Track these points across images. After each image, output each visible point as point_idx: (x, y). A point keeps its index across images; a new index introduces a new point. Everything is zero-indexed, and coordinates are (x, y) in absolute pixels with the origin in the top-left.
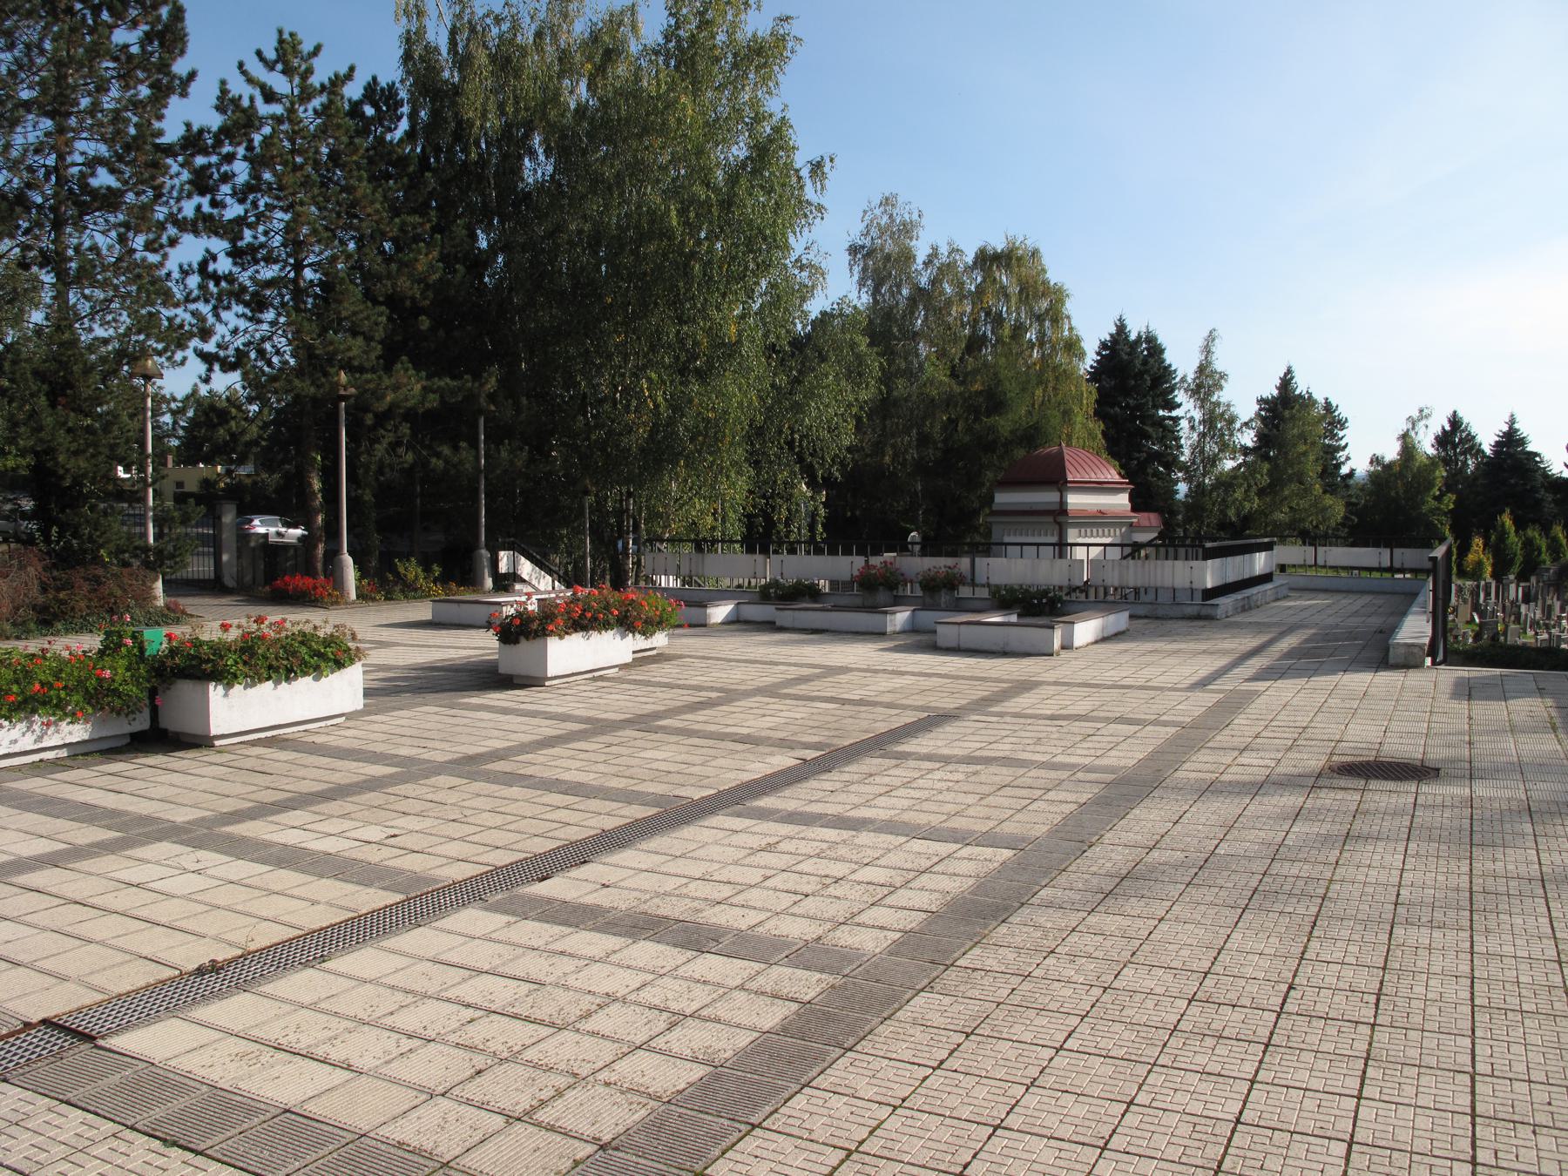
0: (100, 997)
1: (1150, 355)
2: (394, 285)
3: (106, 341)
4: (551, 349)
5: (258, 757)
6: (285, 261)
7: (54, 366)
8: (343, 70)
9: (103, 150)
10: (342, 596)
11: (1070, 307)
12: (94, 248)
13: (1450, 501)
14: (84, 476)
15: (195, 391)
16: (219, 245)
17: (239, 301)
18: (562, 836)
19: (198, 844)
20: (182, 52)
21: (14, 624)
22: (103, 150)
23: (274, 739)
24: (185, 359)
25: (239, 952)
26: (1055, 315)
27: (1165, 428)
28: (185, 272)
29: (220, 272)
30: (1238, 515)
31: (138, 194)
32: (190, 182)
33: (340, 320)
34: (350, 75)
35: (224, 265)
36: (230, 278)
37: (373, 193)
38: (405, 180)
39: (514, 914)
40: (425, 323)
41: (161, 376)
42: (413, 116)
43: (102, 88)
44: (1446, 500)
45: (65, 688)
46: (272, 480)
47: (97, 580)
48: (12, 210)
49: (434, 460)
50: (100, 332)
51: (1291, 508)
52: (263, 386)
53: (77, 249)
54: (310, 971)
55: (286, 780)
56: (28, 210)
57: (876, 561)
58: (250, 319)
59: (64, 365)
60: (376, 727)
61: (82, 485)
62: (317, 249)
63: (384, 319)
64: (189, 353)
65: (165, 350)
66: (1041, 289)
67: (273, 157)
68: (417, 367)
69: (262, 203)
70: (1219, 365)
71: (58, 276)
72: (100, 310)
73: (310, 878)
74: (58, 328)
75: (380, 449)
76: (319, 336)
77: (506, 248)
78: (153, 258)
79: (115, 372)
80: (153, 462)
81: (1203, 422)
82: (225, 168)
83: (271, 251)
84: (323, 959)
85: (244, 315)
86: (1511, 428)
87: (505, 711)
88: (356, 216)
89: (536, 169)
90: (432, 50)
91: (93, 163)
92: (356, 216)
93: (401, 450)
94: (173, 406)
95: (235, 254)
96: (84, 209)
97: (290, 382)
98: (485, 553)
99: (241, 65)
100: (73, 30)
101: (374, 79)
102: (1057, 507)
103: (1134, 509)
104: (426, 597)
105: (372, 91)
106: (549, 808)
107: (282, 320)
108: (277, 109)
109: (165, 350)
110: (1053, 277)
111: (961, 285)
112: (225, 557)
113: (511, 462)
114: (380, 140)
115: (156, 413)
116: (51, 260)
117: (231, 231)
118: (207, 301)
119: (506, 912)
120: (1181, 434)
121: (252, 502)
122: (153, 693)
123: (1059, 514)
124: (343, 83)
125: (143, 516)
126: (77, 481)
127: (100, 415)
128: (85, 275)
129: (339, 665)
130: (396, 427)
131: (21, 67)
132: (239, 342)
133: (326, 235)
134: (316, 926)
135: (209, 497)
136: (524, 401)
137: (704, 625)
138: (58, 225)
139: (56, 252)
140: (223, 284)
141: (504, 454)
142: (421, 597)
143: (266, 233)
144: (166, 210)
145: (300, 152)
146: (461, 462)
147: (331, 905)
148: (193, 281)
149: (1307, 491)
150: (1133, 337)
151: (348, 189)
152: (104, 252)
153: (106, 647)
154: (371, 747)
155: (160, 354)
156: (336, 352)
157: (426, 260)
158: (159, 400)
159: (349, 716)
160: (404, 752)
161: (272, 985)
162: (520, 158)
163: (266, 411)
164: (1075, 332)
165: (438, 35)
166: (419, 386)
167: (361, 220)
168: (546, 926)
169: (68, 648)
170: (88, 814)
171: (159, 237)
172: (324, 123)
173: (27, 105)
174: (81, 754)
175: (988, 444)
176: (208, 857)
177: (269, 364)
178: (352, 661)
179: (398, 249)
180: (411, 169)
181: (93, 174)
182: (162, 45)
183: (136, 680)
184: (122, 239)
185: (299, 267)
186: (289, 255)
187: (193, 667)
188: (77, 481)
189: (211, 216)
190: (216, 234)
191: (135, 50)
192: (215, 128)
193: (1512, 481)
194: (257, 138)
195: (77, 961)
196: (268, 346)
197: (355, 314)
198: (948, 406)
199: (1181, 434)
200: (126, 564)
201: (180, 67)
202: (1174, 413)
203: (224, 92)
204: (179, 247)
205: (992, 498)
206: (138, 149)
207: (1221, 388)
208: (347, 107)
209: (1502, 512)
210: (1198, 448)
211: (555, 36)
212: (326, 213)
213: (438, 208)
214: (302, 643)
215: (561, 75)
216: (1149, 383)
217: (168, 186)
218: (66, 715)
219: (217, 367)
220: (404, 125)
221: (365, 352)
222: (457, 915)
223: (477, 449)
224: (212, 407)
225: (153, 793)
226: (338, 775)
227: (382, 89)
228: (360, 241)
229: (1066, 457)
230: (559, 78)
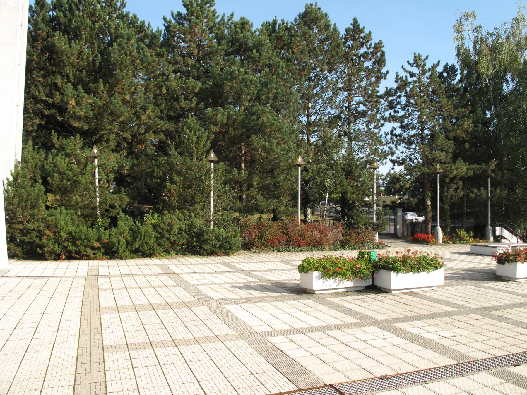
0: (348, 380)
2: (456, 133)
3: (362, 158)
4: (516, 152)
5: (406, 299)
6: (418, 128)
7: (347, 166)
8: (436, 63)
9: (361, 99)
12: (359, 129)
14: (355, 200)
15: (389, 173)
16: (397, 125)
17: (403, 142)
18: (525, 347)
19: (384, 328)
20: (384, 65)
21: (334, 246)
22: (361, 99)
23: (411, 292)
24: (386, 162)
25: (395, 373)
28: (386, 135)
29: (397, 134)
31: (372, 111)
32: (387, 106)
33: (437, 146)
34: (438, 64)
35: (398, 131)
36: (400, 135)
37: (448, 102)
38: (459, 96)
39: (503, 379)
40: (467, 146)
41: (379, 168)
42: (462, 73)
43: (361, 81)
45: (346, 269)
46: (414, 201)
47: (358, 233)
48: (336, 120)
49: (471, 194)
50: (361, 155)
52: (411, 170)
53: (354, 130)
54: (420, 386)
55: (415, 308)
56: (341, 120)
58: (407, 148)
59: (350, 166)
60: (448, 292)
61: (355, 203)
62: (429, 123)
63: (452, 145)
64: (388, 160)
65: (380, 160)
67: (413, 94)
68: (465, 161)
69: (410, 110)
71: (349, 139)
72: (361, 148)
73: (422, 348)
74: (349, 155)
75: (451, 190)
76: (430, 152)
77: (497, 116)
78: (376, 131)
79: (365, 167)
82: (398, 100)
83: (413, 125)
84: (425, 382)
85: (405, 147)
87: (499, 290)
88: (442, 111)
89: (508, 87)
90: (468, 50)
91: (359, 103)
92: (442, 111)
93: (459, 191)
94: (382, 177)
95: (402, 127)
96: (356, 118)
97: (420, 168)
98: (490, 228)
99: (402, 67)
100: (353, 65)
101: (447, 64)
104: (468, 243)
105: (446, 68)
106: (518, 334)
107: (417, 148)
108: (415, 79)
109: (380, 160)
112: (398, 227)
113: (501, 194)
114: (450, 84)
115: (377, 179)
116: (347, 134)
117: (400, 120)
118: (393, 143)
119: (500, 377)
121: (407, 208)
122: (373, 273)
124: (436, 67)
125: (373, 213)
126: (353, 202)
127: (360, 181)
128: (356, 138)
129: (436, 268)
130: (457, 183)
131: (339, 78)
132: (403, 156)
133: (432, 118)
134: (424, 368)
135: (393, 207)
136: (506, 172)
138: (349, 124)
139: (349, 132)
140: (398, 137)
141: (498, 192)
142: (466, 243)
143: (412, 120)
144: (380, 115)
145: (422, 92)
146: (481, 195)
147: (429, 361)
148: (389, 137)
151: (439, 102)
152: (362, 130)
153: (359, 257)
154: (447, 299)
155: (378, 161)
156: (436, 157)
157: (468, 124)
158: (378, 176)
159: (439, 287)
160: (459, 302)
161: (406, 389)
162: (502, 83)
163: (412, 178)
165: (469, 45)
166: (465, 168)
167: (444, 112)
168: (518, 387)
169: (348, 256)
170: (350, 312)
171: (378, 124)
172: (430, 81)
173: (340, 89)
174: (351, 291)
176: (387, 334)
177: (413, 162)
178: (441, 267)
179: (457, 121)
180: (461, 92)
181: (359, 107)
182: (378, 64)
183: (368, 268)
184: (367, 126)
185: (423, 130)
186: (419, 126)
187: (386, 265)
188: (353, 202)
189: (394, 116)
190: (396, 121)
191: (370, 67)
192: (395, 88)
194: (408, 89)
195: (343, 365)
196: (413, 157)
197: (442, 144)
200: (367, 228)
201: (384, 70)
203: (397, 76)
204: (384, 127)
206: (372, 97)
208: (438, 74)
211: (514, 37)
212: (431, 111)
213: (471, 105)
214: (423, 260)
215: (517, 51)
217: (381, 108)
218: (346, 278)
219: (396, 164)
220: (458, 77)
221: (446, 157)
222: (479, 375)
223: (487, 189)
224: (395, 177)
225: (371, 308)
226: (434, 309)
227: (450, 67)
228: (444, 119)
230: (516, 51)
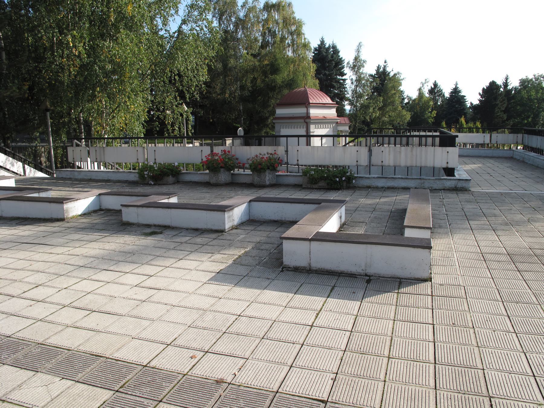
1: (334, 53)
11: (305, 30)
13: (434, 113)
26: (299, 33)
27: (340, 83)
30: (370, 119)
44: (433, 113)
51: (389, 116)
57: (218, 150)
66: (292, 21)
70: (363, 57)
80: (236, 124)
81: (356, 80)
86: (456, 86)
102: (305, 115)
103: (338, 116)
110: (298, 16)
111: (258, 17)
120: (346, 86)
123: (306, 119)
137: (62, 220)
149: (395, 109)
150: (327, 46)
164: (307, 40)
175: (272, 88)
193: (457, 106)
198: (253, 71)
199: (346, 86)
202: (344, 78)
205: (275, 112)
207: (363, 67)
209: (461, 117)
210: (354, 92)
216: (334, 65)
229: (308, 92)
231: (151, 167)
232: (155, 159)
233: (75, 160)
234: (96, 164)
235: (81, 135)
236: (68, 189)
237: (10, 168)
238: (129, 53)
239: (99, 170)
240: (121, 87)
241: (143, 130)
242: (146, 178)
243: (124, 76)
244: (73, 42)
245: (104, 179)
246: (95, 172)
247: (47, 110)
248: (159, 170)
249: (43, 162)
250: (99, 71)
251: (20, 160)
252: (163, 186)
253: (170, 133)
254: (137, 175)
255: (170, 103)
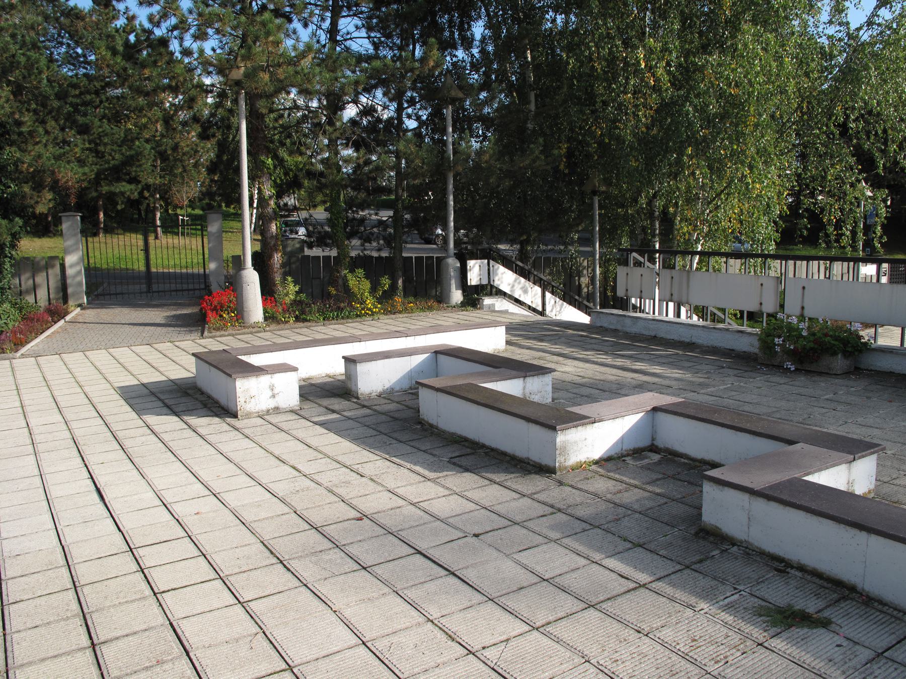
10: (28, 233)
98: (453, 263)
231: (790, 328)
232: (803, 308)
233: (629, 294)
234: (671, 305)
235: (653, 240)
236: (602, 358)
237: (520, 296)
238: (757, 74)
239: (677, 320)
240: (735, 147)
241: (776, 234)
242: (777, 352)
243: (745, 123)
244: (647, 59)
245: (682, 339)
246: (665, 324)
247: (594, 193)
248: (812, 338)
249: (583, 286)
250: (694, 115)
251: (537, 281)
252: (816, 378)
253: (830, 241)
254: (756, 343)
255: (836, 179)
